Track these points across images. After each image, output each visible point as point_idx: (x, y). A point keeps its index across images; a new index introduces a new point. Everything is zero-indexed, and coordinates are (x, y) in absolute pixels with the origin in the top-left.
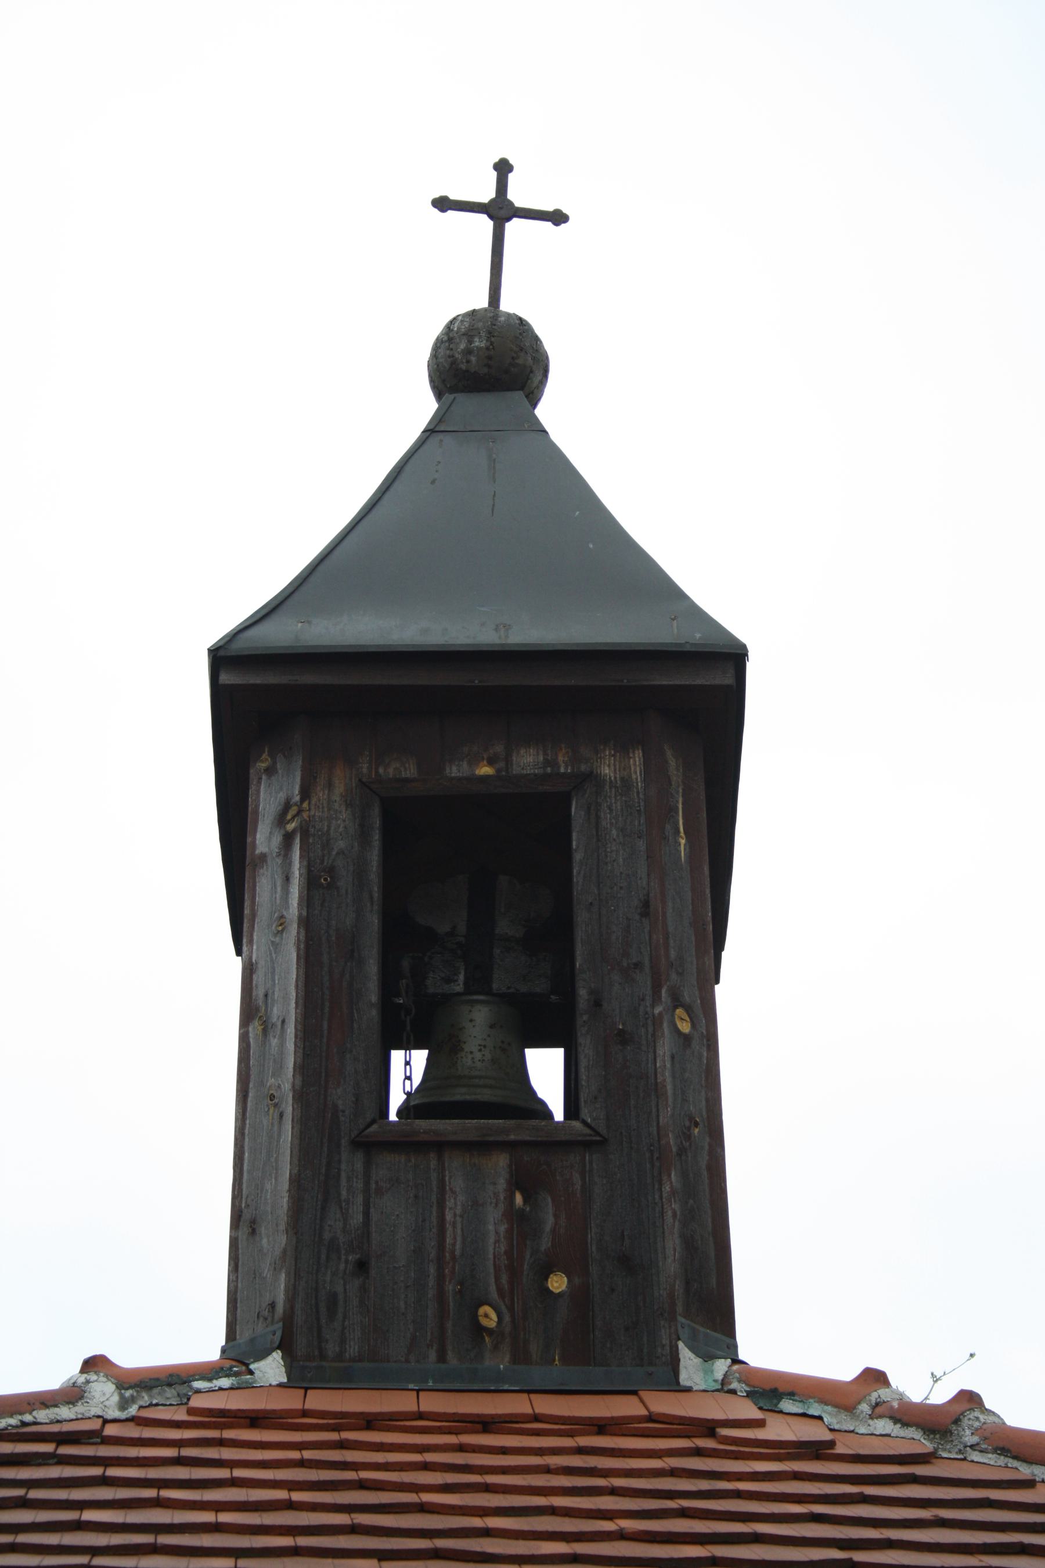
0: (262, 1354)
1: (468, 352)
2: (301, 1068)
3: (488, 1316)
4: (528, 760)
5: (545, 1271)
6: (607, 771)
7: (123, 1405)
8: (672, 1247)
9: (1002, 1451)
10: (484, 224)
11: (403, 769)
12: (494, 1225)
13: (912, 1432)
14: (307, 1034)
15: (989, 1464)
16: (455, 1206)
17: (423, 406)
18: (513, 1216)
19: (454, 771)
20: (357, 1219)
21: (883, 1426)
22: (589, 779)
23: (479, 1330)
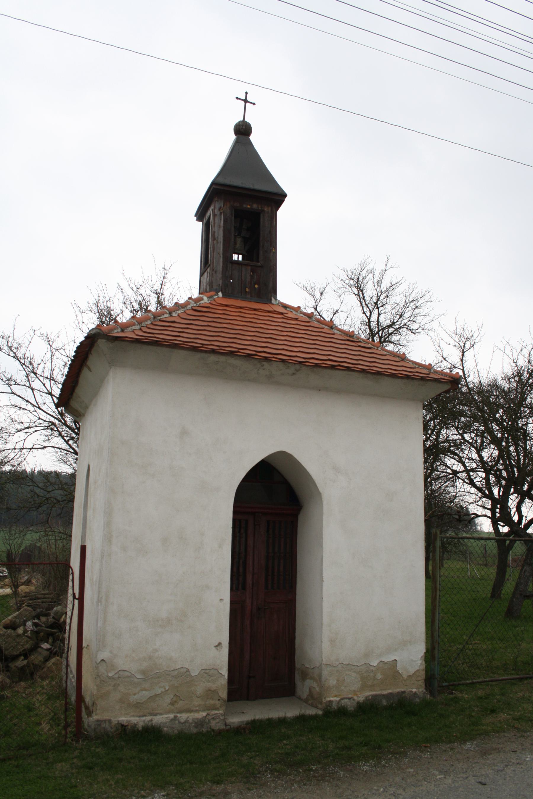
0: (219, 292)
1: (242, 128)
2: (223, 250)
3: (247, 290)
4: (255, 206)
5: (255, 284)
6: (266, 209)
7: (208, 300)
8: (271, 283)
9: (318, 322)
10: (243, 103)
11: (237, 204)
12: (248, 278)
13: (306, 317)
14: (224, 245)
15: (316, 324)
16: (244, 273)
17: (233, 137)
18: (251, 275)
19: (245, 206)
20: (230, 273)
21: (302, 315)
22: (263, 211)
23: (246, 291)
